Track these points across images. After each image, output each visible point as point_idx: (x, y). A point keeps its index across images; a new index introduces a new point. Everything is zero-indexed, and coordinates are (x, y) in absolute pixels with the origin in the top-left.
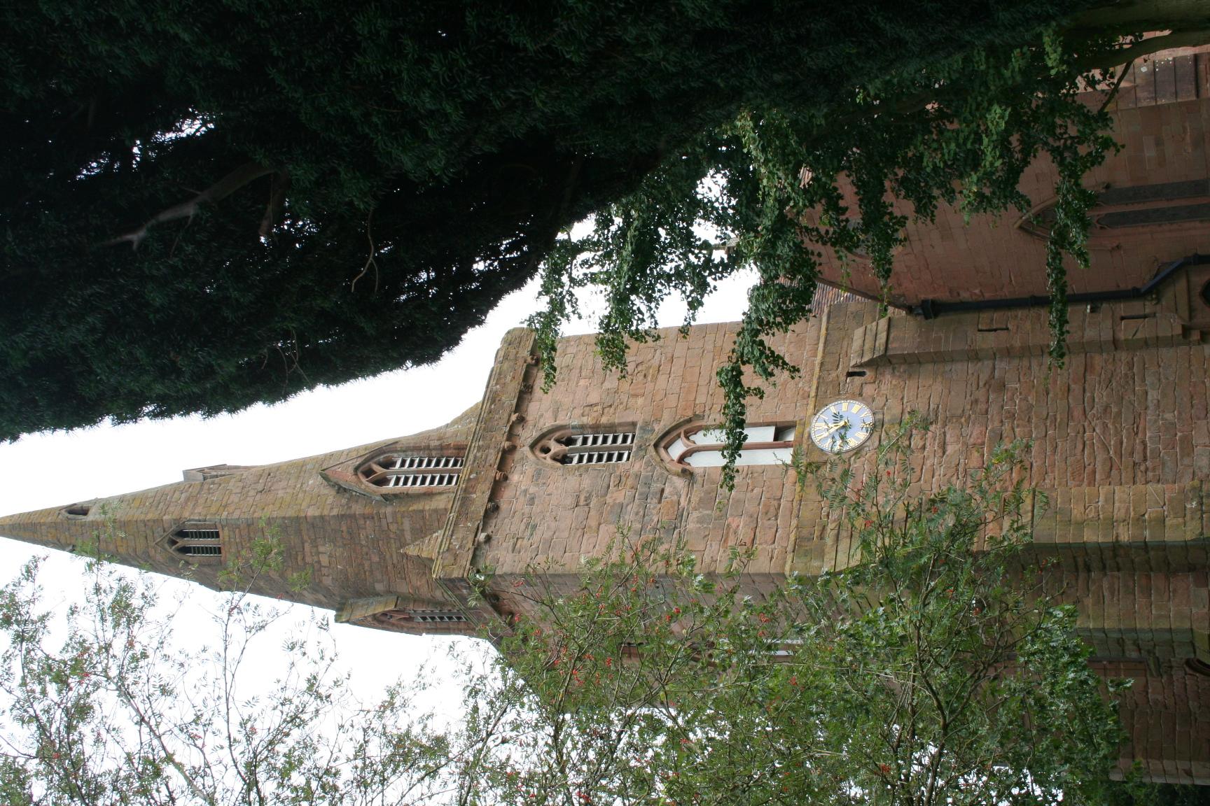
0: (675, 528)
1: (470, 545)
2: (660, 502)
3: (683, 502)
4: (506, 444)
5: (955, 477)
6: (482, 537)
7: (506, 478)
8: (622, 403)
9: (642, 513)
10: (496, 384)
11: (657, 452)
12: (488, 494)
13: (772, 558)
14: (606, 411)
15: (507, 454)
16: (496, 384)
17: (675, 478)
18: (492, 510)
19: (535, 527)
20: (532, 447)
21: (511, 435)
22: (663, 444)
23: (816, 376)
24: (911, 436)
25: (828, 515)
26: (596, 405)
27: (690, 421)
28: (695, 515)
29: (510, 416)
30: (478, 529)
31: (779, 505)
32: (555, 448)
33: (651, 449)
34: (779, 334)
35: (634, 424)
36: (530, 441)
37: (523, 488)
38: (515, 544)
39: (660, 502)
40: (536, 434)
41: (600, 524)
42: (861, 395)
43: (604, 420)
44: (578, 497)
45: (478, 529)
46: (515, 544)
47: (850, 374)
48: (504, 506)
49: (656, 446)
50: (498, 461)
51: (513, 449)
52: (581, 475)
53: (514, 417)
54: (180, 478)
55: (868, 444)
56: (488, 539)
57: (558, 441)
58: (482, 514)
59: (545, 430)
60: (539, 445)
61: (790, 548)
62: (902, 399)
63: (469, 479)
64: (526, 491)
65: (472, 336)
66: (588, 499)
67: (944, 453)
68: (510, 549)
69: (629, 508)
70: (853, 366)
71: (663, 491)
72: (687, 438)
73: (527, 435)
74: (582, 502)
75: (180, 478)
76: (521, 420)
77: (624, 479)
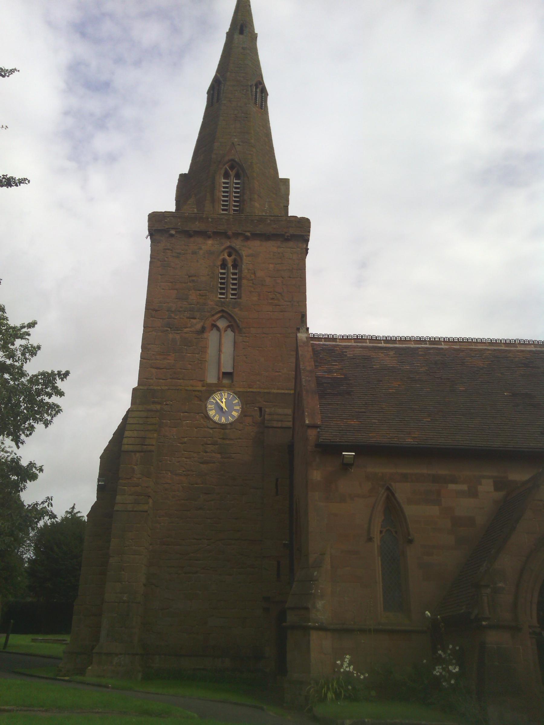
0: (171, 328)
1: (167, 227)
2: (187, 318)
3: (185, 330)
4: (230, 233)
5: (184, 470)
6: (173, 232)
7: (209, 237)
8: (254, 289)
9: (181, 309)
10: (271, 220)
11: (219, 312)
12: (198, 230)
13: (147, 379)
14: (251, 281)
15: (224, 235)
16: (271, 220)
17: (202, 324)
18: (189, 234)
19: (177, 257)
20: (230, 247)
21: (236, 235)
22: (224, 314)
23: (262, 390)
24: (214, 445)
25: (167, 405)
26: (255, 276)
27: (238, 327)
28: (178, 337)
29: (249, 232)
30: (177, 229)
31: (179, 379)
32: (230, 260)
33: (220, 309)
34: (47, 504)
35: (240, 298)
36: (233, 245)
37: (203, 247)
38: (168, 249)
39: (187, 318)
40: (237, 247)
41: (177, 289)
42: (245, 416)
43: (244, 282)
44: (195, 276)
45: (177, 229)
46: (168, 249)
47: (260, 409)
48: (192, 240)
49: (223, 311)
50: (219, 231)
51: (228, 237)
52: (208, 275)
53: (248, 234)
54: (282, 175)
55: (211, 422)
56: (172, 236)
57: (235, 260)
58: (186, 229)
59: (240, 252)
60: (231, 251)
61: (152, 387)
62: (240, 438)
63: (208, 218)
64: (201, 249)
65: (230, 173)
66: (193, 281)
67: (201, 463)
68: (166, 248)
69: (185, 303)
70: (265, 410)
71: (195, 318)
72: (228, 327)
73: (237, 243)
74: (191, 278)
75: (282, 175)
76: (247, 239)
77: (204, 297)
